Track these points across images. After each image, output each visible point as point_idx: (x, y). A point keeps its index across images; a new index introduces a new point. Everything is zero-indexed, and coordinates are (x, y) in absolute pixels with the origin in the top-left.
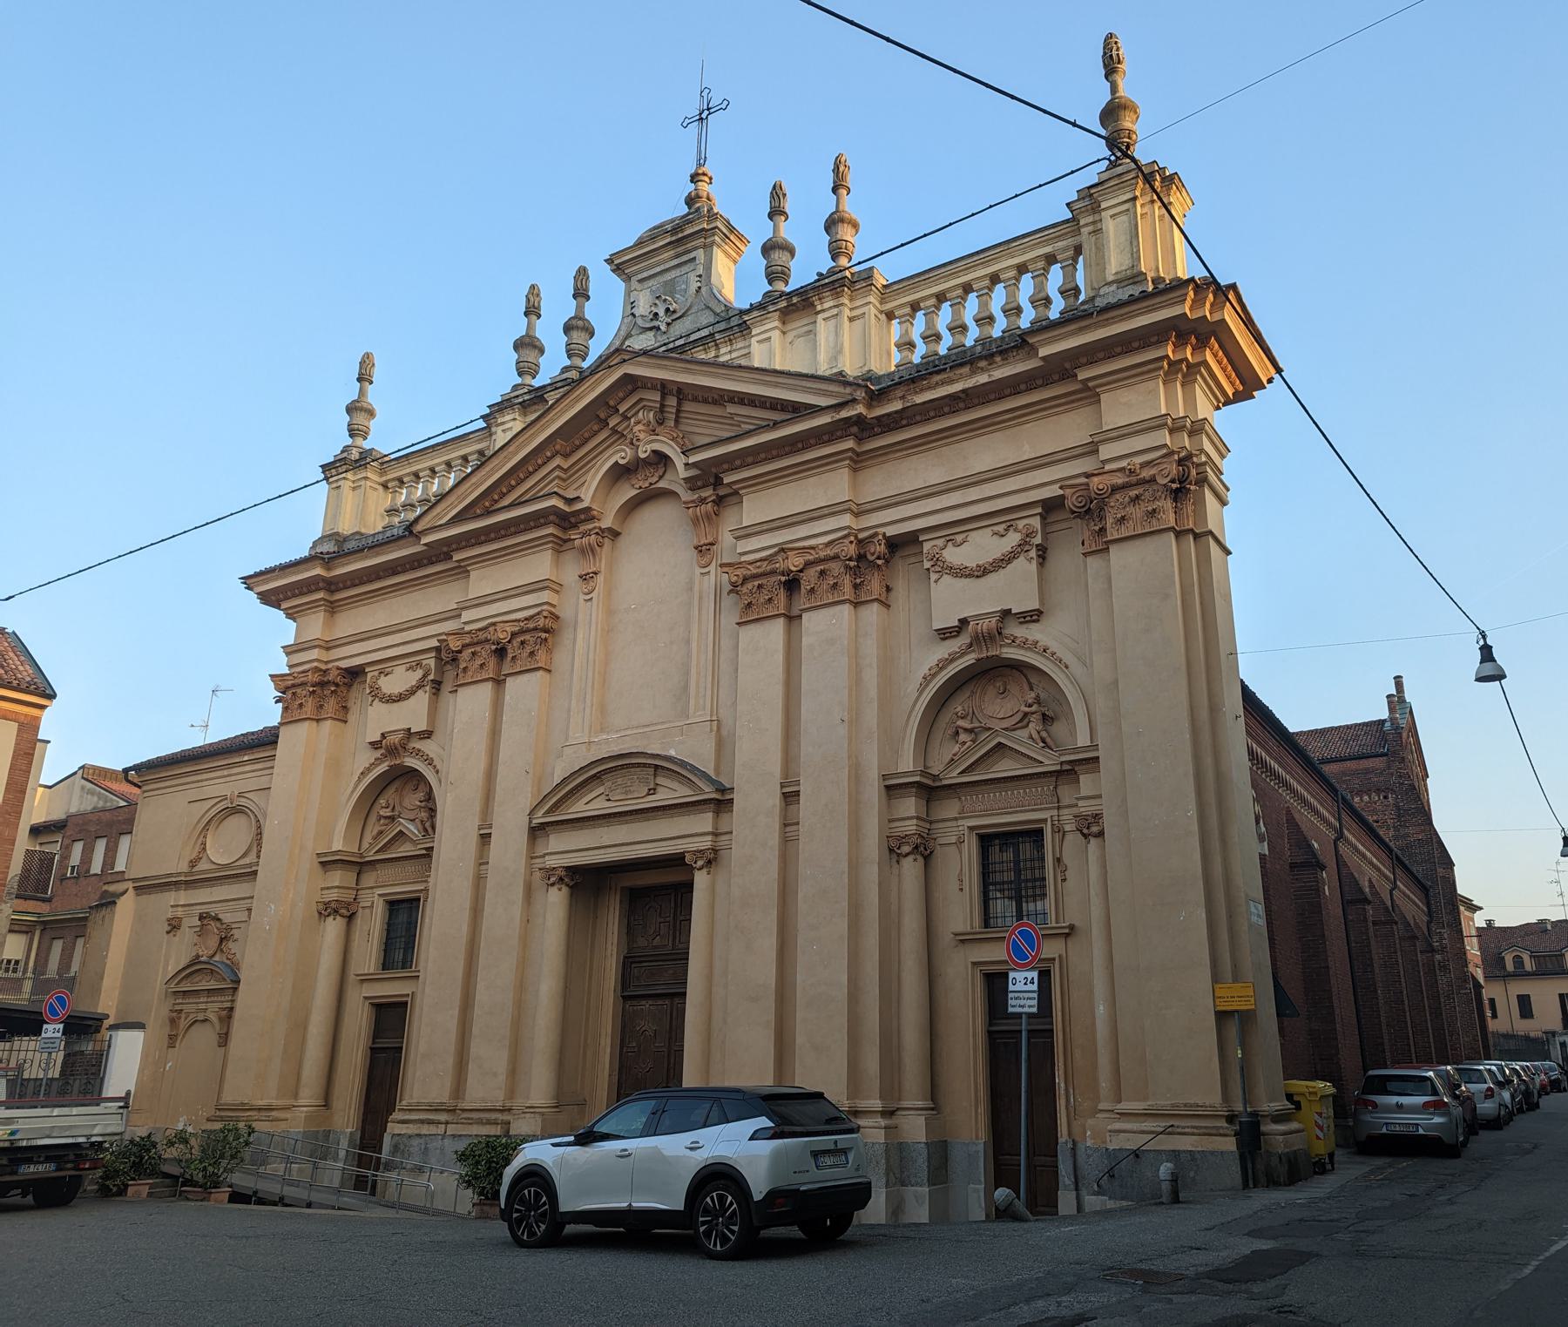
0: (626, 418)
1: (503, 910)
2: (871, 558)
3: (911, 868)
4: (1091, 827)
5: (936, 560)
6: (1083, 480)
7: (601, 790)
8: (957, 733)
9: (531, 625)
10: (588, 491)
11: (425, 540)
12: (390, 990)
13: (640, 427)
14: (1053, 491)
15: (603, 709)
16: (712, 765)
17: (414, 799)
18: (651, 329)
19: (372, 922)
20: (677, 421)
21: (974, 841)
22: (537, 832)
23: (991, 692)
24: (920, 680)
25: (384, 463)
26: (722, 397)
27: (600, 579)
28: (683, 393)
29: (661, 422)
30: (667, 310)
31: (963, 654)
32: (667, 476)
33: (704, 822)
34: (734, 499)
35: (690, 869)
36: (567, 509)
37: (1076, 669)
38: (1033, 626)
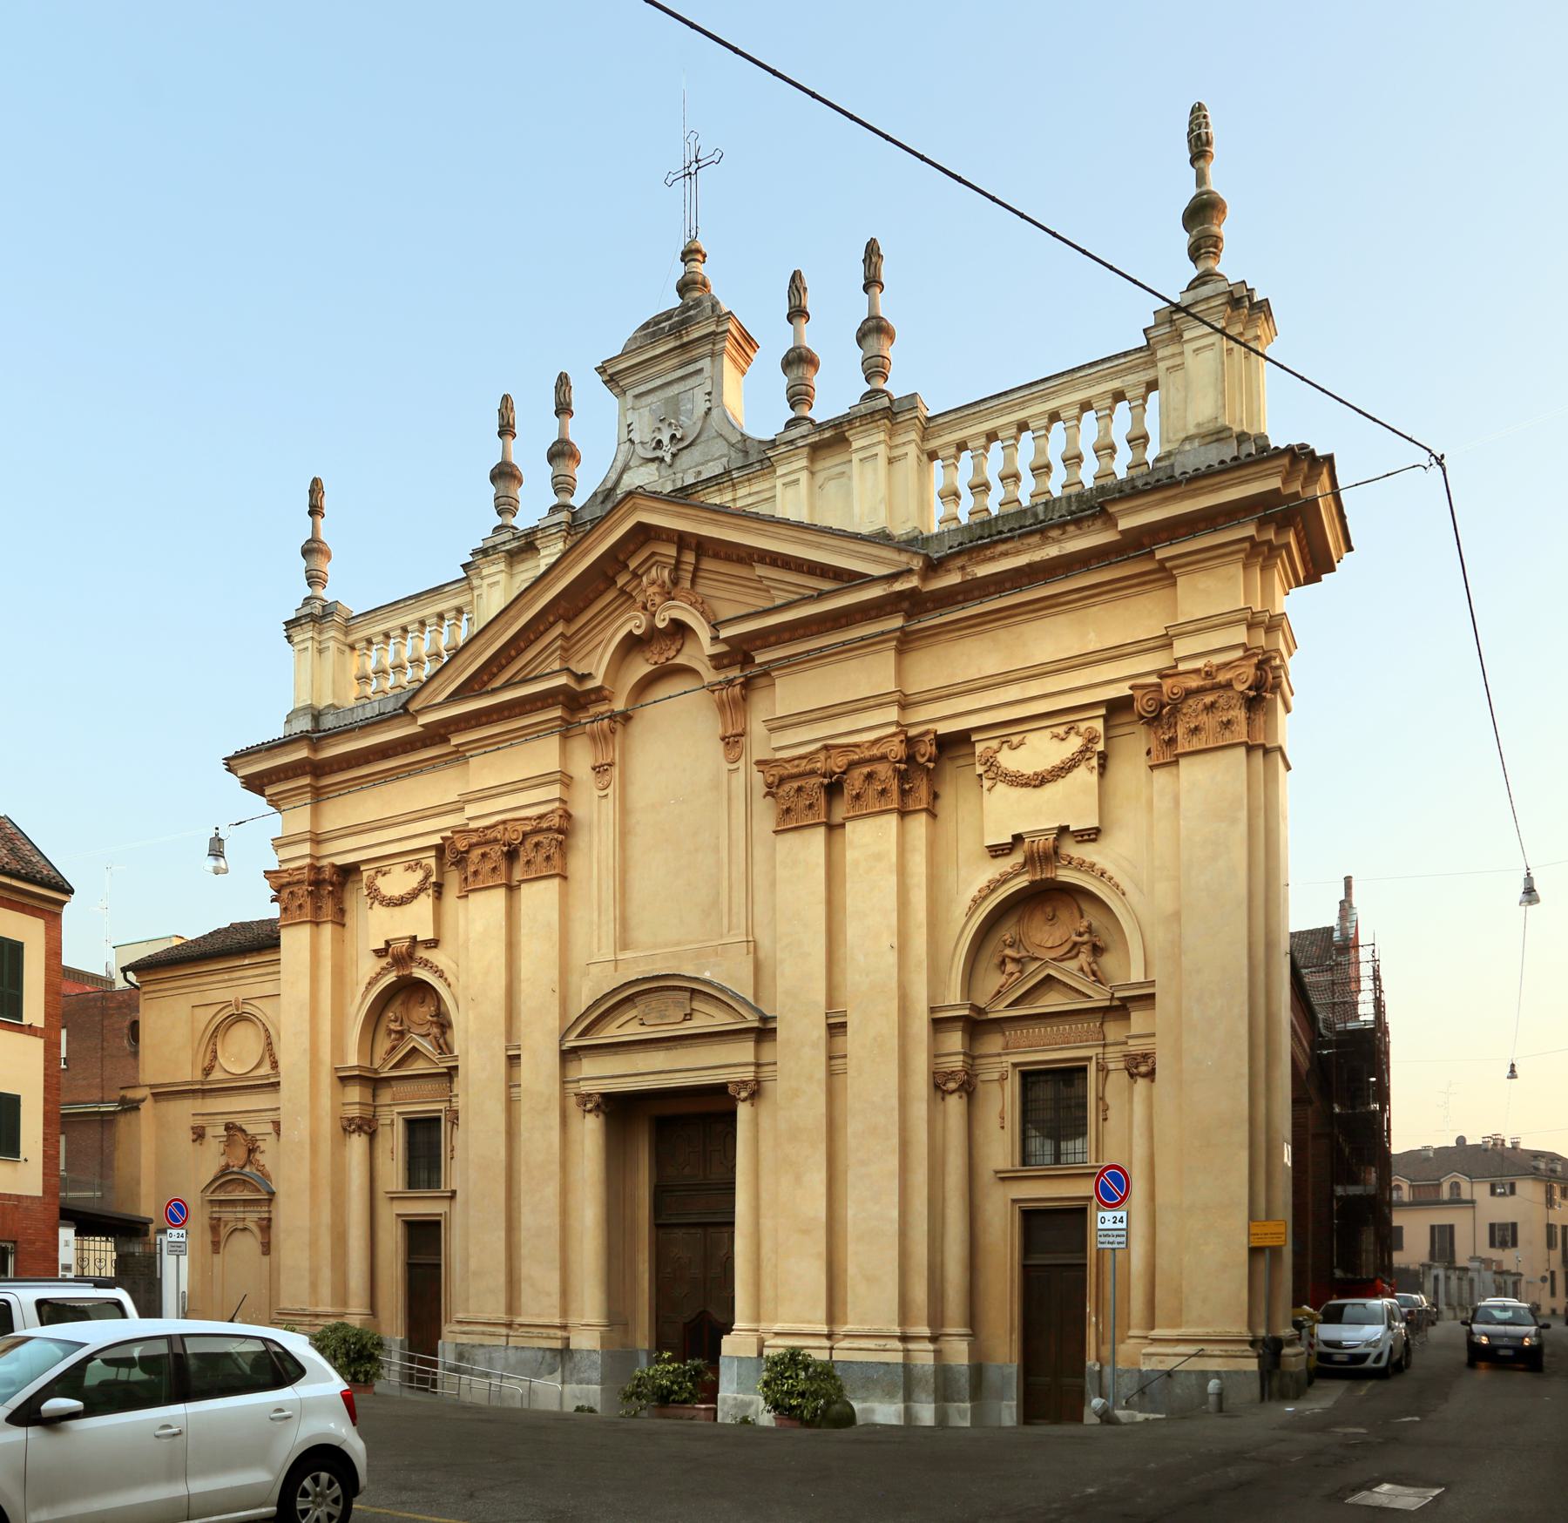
0: (636, 575)
1: (539, 1136)
2: (922, 760)
3: (955, 1105)
4: (1141, 1067)
5: (991, 763)
6: (1154, 679)
7: (633, 1013)
8: (1003, 963)
9: (544, 825)
10: (597, 664)
11: (423, 720)
12: (422, 1208)
13: (654, 589)
14: (1123, 690)
15: (624, 924)
16: (751, 992)
17: (423, 1012)
18: (652, 460)
19: (393, 1141)
20: (693, 582)
21: (1017, 1078)
22: (568, 1055)
23: (1039, 918)
24: (969, 903)
25: (349, 624)
26: (751, 556)
27: (616, 771)
28: (703, 547)
29: (675, 582)
30: (673, 437)
31: (1017, 875)
32: (686, 649)
33: (744, 1051)
34: (763, 681)
35: (733, 1101)
36: (578, 689)
37: (1133, 896)
38: (1090, 847)
